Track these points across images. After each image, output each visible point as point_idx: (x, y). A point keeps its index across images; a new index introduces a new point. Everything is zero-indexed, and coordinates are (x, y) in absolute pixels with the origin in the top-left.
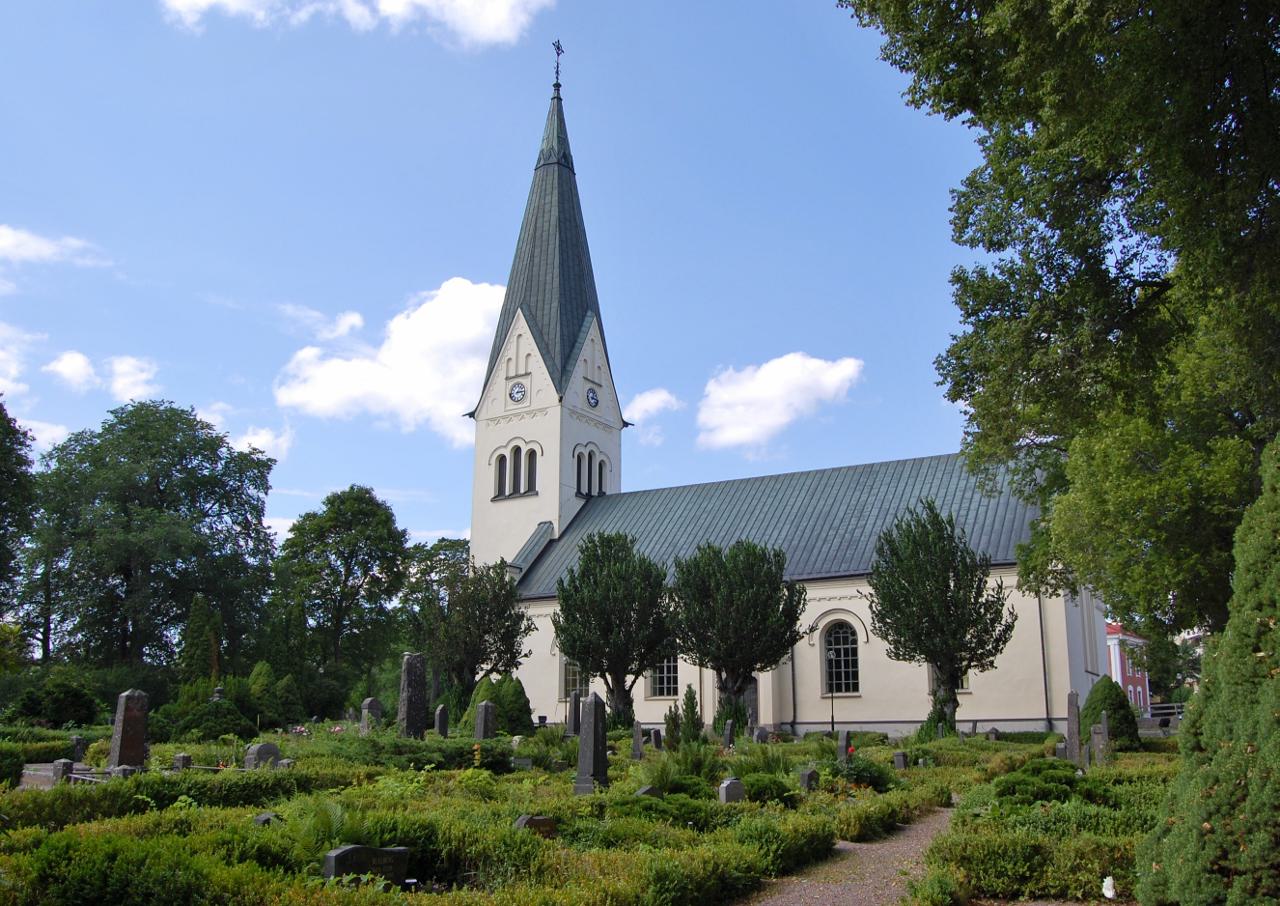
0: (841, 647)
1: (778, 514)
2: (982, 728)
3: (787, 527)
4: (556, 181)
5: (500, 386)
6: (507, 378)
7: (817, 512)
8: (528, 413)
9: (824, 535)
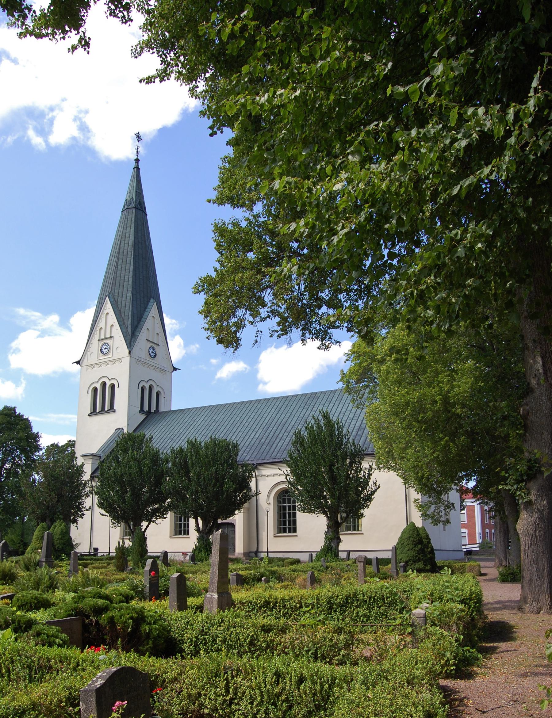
0: (282, 505)
1: (256, 423)
2: (353, 556)
3: (260, 431)
4: (133, 218)
5: (95, 345)
6: (99, 340)
7: (279, 421)
8: (111, 361)
9: (281, 435)
